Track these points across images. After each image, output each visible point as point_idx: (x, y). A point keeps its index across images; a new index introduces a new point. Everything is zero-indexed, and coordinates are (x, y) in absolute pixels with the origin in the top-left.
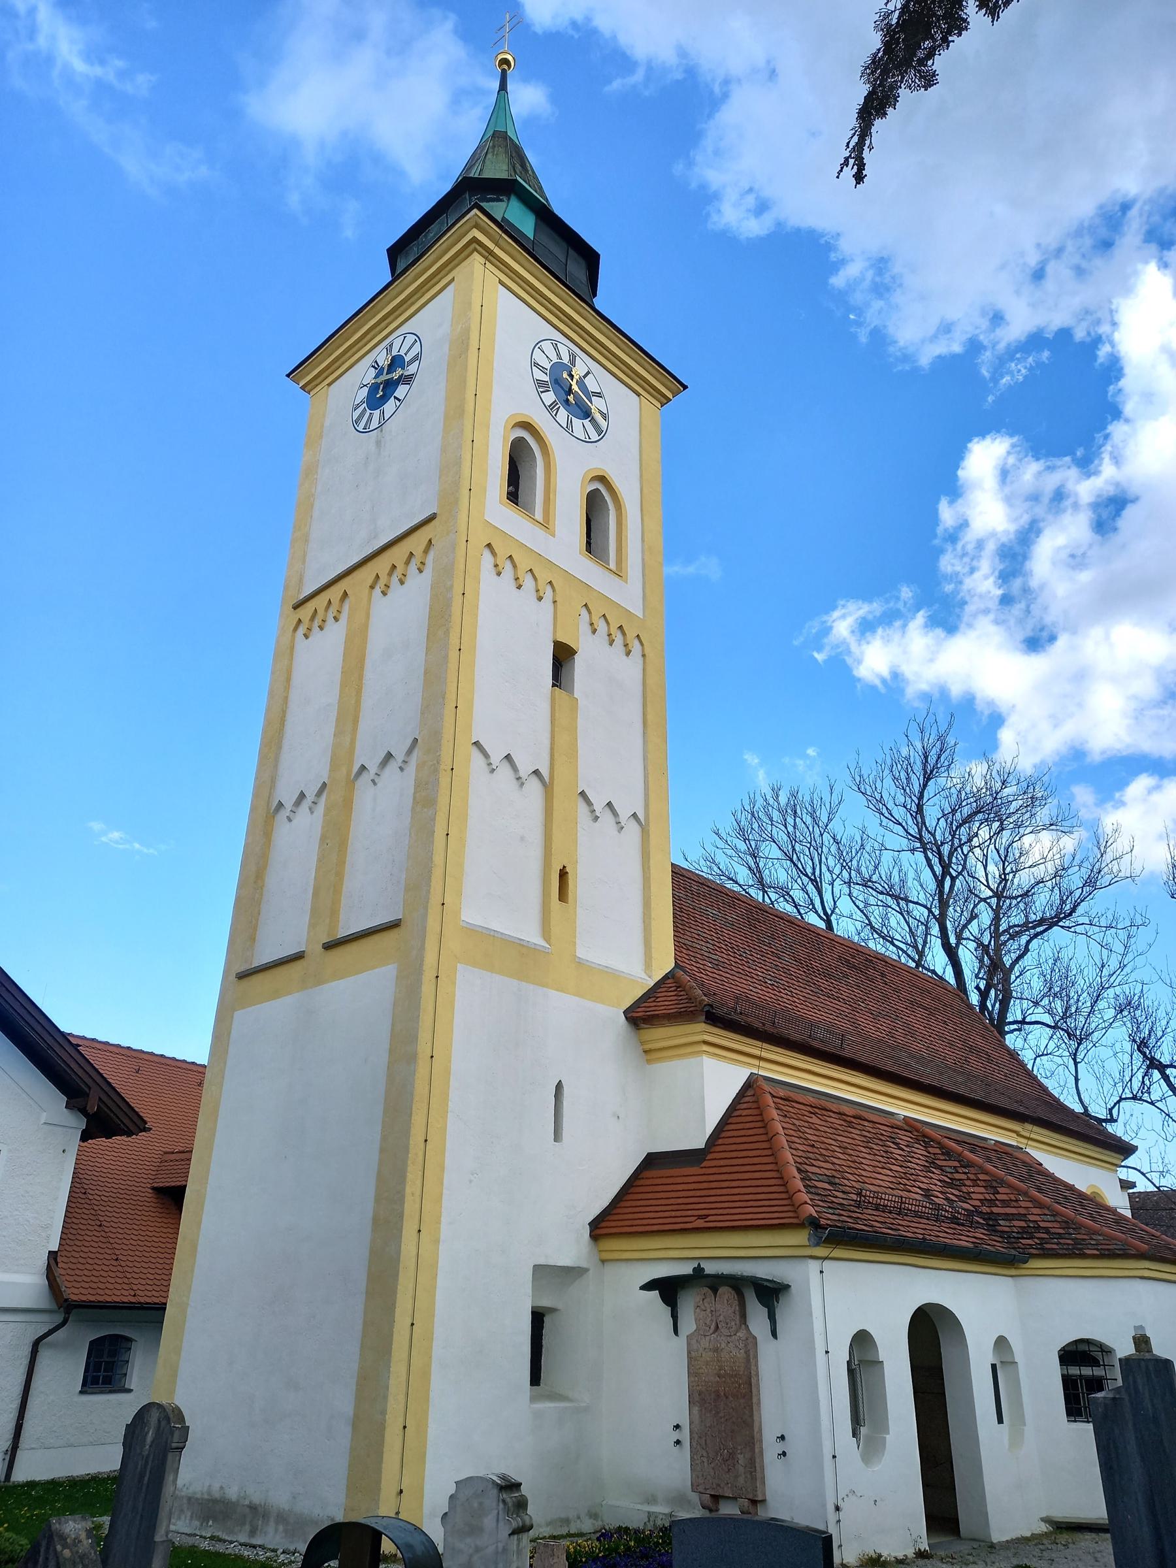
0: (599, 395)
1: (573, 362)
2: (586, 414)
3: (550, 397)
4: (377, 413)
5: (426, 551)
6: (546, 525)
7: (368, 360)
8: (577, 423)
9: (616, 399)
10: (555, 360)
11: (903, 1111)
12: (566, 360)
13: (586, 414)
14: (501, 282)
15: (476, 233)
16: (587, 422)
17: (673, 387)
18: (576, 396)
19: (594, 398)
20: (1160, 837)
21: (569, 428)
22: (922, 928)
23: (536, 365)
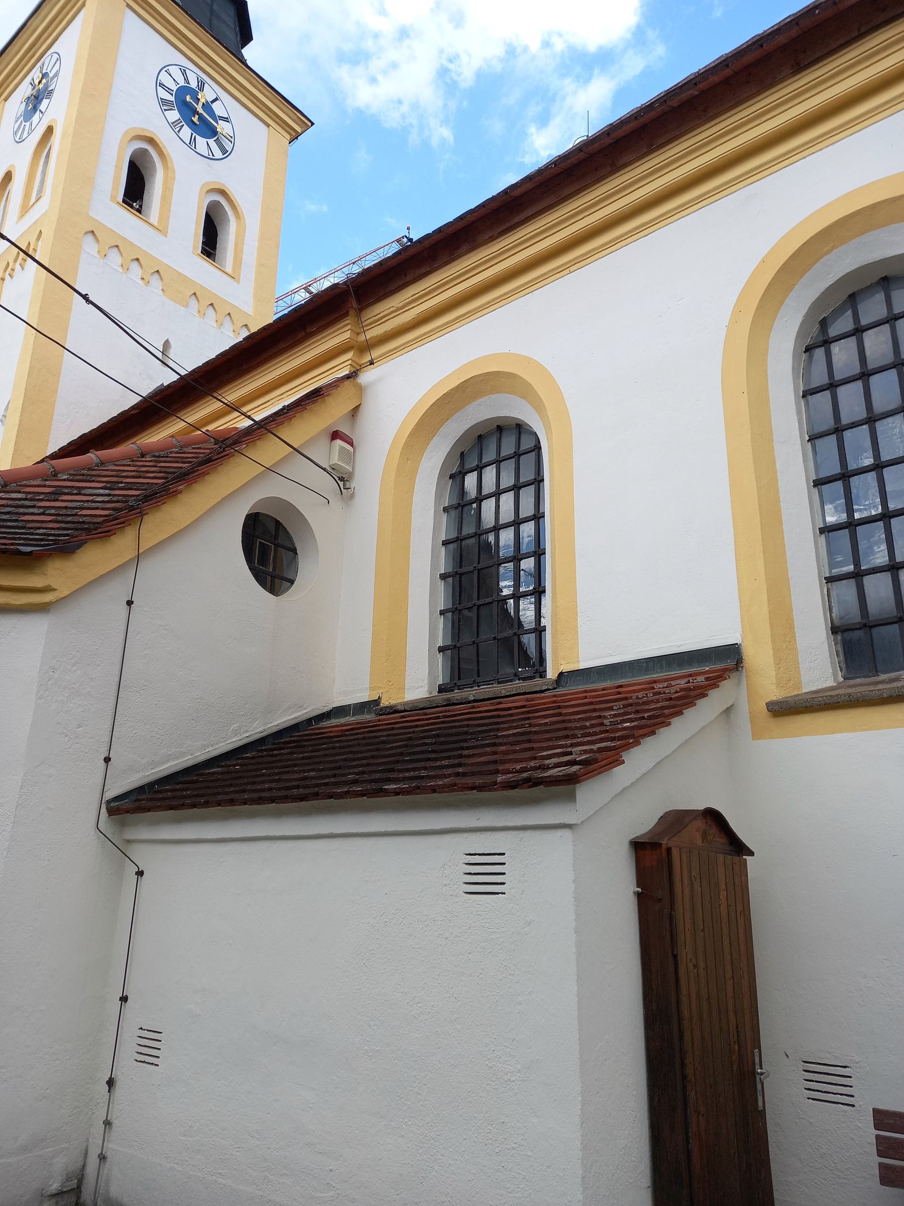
0: (226, 120)
2: (212, 132)
3: (174, 115)
4: (28, 124)
5: (38, 239)
6: (162, 229)
7: (28, 79)
8: (201, 141)
10: (182, 83)
12: (194, 84)
13: (212, 132)
14: (128, 6)
16: (211, 142)
18: (201, 118)
21: (192, 144)
22: (368, 632)
23: (162, 85)
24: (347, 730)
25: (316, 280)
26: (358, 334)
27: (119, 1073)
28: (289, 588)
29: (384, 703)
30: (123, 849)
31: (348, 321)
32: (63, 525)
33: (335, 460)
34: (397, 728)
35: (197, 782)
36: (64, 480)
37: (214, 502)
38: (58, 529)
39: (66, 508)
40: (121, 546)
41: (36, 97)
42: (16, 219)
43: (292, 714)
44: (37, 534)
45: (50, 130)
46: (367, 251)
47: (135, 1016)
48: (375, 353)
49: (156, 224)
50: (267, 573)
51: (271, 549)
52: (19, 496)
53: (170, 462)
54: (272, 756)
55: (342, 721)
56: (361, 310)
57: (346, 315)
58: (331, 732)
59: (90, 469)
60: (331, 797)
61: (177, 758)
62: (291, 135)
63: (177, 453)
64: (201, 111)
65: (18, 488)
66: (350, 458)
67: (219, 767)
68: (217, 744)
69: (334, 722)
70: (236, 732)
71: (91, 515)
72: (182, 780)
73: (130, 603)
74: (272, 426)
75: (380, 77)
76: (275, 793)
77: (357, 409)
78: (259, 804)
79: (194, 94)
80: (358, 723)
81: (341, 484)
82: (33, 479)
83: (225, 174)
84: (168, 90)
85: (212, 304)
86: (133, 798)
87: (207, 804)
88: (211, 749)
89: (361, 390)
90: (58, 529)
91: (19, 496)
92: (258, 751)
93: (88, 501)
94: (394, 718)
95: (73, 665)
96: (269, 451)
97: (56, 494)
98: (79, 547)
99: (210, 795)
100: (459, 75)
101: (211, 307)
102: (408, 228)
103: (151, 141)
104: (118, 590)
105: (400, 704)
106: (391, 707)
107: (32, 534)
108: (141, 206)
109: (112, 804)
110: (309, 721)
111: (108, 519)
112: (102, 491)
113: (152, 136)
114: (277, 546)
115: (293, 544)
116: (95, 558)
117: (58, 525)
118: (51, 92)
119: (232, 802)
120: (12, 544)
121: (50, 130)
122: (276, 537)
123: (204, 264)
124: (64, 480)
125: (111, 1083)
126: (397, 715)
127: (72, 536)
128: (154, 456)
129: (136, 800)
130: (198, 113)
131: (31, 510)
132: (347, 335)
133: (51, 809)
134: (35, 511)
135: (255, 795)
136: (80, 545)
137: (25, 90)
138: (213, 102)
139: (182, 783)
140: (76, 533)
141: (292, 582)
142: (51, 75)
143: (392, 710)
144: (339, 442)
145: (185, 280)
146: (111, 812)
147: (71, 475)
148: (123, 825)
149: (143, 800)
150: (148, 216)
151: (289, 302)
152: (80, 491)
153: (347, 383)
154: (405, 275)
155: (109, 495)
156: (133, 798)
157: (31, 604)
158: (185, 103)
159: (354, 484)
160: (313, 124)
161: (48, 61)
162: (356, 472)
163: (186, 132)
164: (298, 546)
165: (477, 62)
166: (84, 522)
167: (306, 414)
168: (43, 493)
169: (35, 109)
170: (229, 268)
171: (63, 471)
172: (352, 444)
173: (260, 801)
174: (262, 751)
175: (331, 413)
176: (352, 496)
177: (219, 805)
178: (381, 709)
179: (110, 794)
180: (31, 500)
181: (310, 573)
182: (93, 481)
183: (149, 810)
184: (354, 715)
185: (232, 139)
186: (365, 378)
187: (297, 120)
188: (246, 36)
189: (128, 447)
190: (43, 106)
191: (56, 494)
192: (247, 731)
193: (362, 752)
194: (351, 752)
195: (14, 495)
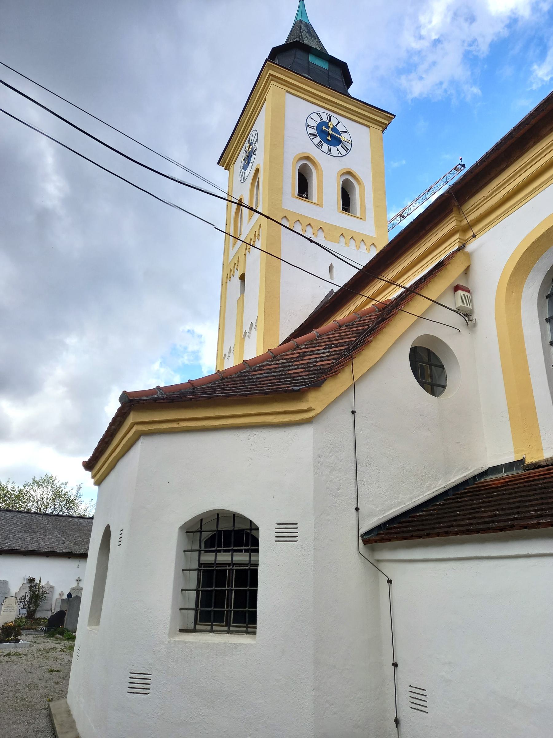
1: (329, 120)
3: (318, 140)
8: (334, 149)
9: (356, 133)
10: (319, 121)
11: (490, 477)
12: (325, 119)
14: (287, 91)
15: (270, 72)
16: (339, 147)
17: (266, 70)
18: (332, 136)
19: (342, 135)
20: (241, 199)
21: (329, 152)
23: (309, 126)
24: (506, 482)
25: (405, 209)
26: (461, 221)
27: (401, 715)
28: (443, 391)
29: (528, 461)
30: (376, 565)
31: (453, 215)
32: (310, 373)
33: (460, 303)
34: (549, 478)
35: (412, 521)
36: (303, 349)
37: (390, 344)
38: (308, 375)
39: (308, 363)
40: (344, 380)
41: (248, 157)
42: (247, 222)
43: (462, 473)
44: (299, 380)
45: (257, 170)
46: (436, 181)
47: (406, 677)
48: (475, 230)
49: (316, 202)
50: (428, 384)
51: (429, 367)
52: (283, 361)
53: (357, 327)
54: (458, 502)
55: (499, 476)
56: (459, 207)
57: (451, 211)
58: (494, 484)
59: (315, 340)
60: (525, 528)
61: (396, 507)
62: (382, 127)
63: (359, 321)
64: (331, 132)
65: (281, 357)
66: (469, 300)
67: (422, 511)
68: (418, 496)
69: (491, 477)
70: (429, 488)
71: (323, 365)
72: (402, 520)
73: (353, 412)
74: (417, 290)
75: (424, 76)
76: (475, 527)
77: (468, 269)
78: (468, 534)
79: (326, 125)
80: (513, 477)
81: (466, 318)
82: (263, 362)
83: (351, 162)
84: (313, 127)
85: (352, 237)
86: (375, 533)
87: (429, 535)
88: (415, 500)
89: (469, 256)
90: (308, 375)
91: (283, 361)
92: (445, 500)
93: (319, 357)
94: (541, 471)
95: (330, 453)
96: (419, 305)
97: (301, 357)
98: (323, 383)
99: (431, 529)
100: (479, 51)
101: (352, 239)
102: (461, 159)
103: (308, 158)
104: (345, 406)
105: (543, 461)
106: (535, 464)
107: (296, 380)
108: (307, 195)
109: (365, 537)
110: (474, 478)
111: (333, 365)
112: (324, 351)
113: (305, 155)
114: (431, 365)
115: (441, 362)
116: (333, 388)
117: (308, 373)
118: (255, 151)
119: (447, 534)
120: (288, 387)
121: (257, 170)
122: (429, 359)
123: (345, 216)
124: (303, 349)
125: (397, 721)
126: (541, 469)
127: (317, 378)
128: (347, 326)
129: (378, 534)
130: (330, 134)
131: (291, 368)
132: (454, 224)
133: (332, 541)
134: (293, 367)
135: (464, 528)
136: (323, 382)
137: (243, 155)
138: (336, 125)
139: (403, 522)
140: (319, 375)
141: (444, 387)
142: (254, 142)
143: (537, 466)
144: (460, 292)
145: (336, 228)
146: (365, 542)
147: (305, 345)
148: (373, 550)
149: (382, 534)
150: (312, 199)
151: (391, 226)
152: (313, 353)
153: (459, 253)
154: (490, 174)
155: (329, 352)
156: (375, 533)
157: (303, 419)
158: (323, 131)
159: (475, 316)
160: (395, 116)
161: (252, 137)
162: (475, 308)
163: (325, 146)
164: (444, 363)
165: (489, 39)
166: (320, 369)
167: (436, 279)
168: (294, 358)
169: (248, 163)
170: (359, 215)
171: (301, 344)
172: (468, 291)
173: (468, 532)
174: (447, 500)
175: (452, 274)
176: (475, 325)
177: (438, 536)
178: (528, 466)
179: (363, 530)
180: (289, 362)
181: (457, 379)
182: (318, 346)
183: (390, 540)
184: (506, 472)
185: (350, 142)
186: (470, 248)
187: (386, 117)
188: (349, 82)
189: (330, 324)
190: (252, 160)
191: (301, 357)
192: (435, 487)
193: (530, 496)
194: (521, 496)
195: (280, 361)
